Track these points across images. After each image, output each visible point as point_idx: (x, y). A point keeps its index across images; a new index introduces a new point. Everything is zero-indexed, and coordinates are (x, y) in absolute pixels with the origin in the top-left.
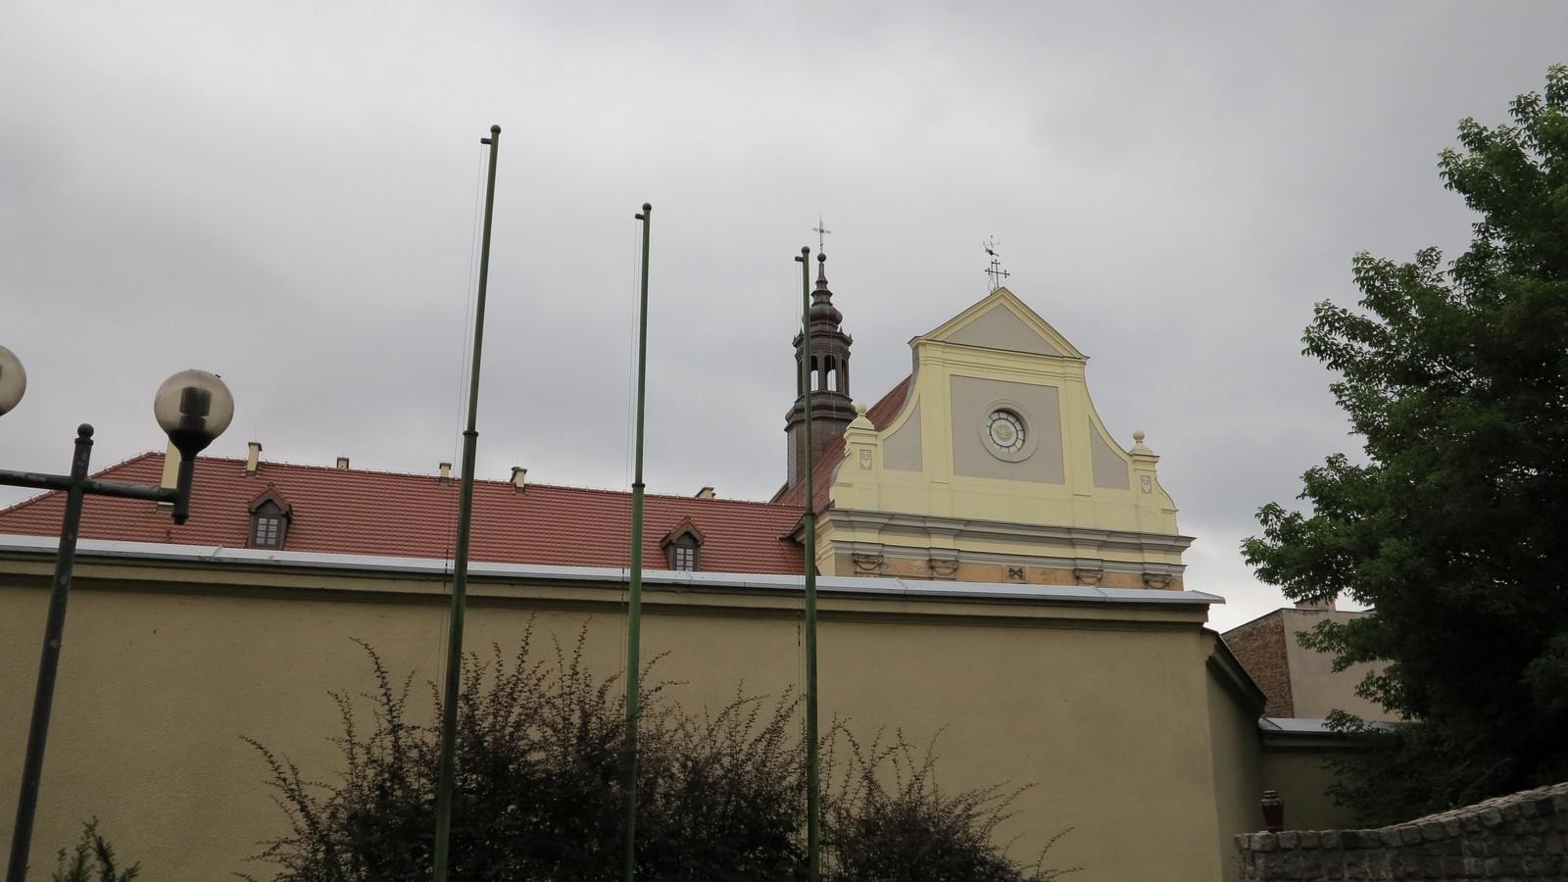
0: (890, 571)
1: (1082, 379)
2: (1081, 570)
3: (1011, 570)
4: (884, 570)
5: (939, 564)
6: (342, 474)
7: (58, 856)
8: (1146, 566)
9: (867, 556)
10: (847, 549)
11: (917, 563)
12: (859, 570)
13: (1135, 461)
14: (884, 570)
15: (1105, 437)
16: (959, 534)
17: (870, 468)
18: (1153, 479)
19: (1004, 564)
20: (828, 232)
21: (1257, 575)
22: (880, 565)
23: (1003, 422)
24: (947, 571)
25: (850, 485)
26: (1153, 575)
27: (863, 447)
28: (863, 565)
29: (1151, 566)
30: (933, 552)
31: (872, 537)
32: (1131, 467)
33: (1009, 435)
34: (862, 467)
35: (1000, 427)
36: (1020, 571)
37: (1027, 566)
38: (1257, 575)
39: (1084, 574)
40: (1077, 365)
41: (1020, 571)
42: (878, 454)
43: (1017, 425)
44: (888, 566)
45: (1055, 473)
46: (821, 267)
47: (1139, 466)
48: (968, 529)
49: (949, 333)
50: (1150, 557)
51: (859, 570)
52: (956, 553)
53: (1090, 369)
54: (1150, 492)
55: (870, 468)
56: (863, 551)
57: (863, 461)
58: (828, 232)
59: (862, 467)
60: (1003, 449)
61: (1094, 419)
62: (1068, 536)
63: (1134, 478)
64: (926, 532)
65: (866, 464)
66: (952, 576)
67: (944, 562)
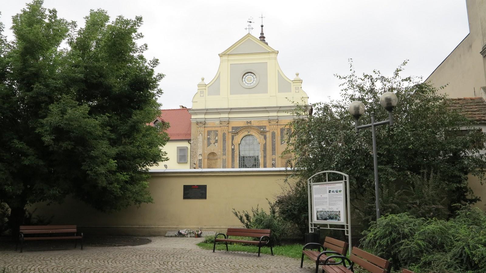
0: (208, 126)
1: (276, 59)
4: (206, 126)
8: (269, 117)
9: (201, 122)
11: (217, 123)
13: (293, 82)
16: (229, 113)
20: (262, 15)
25: (197, 102)
26: (272, 120)
27: (201, 90)
28: (199, 125)
30: (221, 119)
31: (202, 116)
33: (251, 80)
35: (248, 78)
36: (250, 122)
37: (253, 120)
39: (272, 121)
43: (252, 75)
44: (208, 124)
46: (262, 29)
47: (295, 84)
49: (231, 51)
50: (271, 114)
51: (198, 126)
52: (277, 117)
53: (279, 56)
55: (203, 96)
58: (262, 15)
59: (296, 92)
61: (279, 71)
63: (293, 88)
64: (219, 113)
65: (202, 95)
66: (227, 126)
67: (225, 121)
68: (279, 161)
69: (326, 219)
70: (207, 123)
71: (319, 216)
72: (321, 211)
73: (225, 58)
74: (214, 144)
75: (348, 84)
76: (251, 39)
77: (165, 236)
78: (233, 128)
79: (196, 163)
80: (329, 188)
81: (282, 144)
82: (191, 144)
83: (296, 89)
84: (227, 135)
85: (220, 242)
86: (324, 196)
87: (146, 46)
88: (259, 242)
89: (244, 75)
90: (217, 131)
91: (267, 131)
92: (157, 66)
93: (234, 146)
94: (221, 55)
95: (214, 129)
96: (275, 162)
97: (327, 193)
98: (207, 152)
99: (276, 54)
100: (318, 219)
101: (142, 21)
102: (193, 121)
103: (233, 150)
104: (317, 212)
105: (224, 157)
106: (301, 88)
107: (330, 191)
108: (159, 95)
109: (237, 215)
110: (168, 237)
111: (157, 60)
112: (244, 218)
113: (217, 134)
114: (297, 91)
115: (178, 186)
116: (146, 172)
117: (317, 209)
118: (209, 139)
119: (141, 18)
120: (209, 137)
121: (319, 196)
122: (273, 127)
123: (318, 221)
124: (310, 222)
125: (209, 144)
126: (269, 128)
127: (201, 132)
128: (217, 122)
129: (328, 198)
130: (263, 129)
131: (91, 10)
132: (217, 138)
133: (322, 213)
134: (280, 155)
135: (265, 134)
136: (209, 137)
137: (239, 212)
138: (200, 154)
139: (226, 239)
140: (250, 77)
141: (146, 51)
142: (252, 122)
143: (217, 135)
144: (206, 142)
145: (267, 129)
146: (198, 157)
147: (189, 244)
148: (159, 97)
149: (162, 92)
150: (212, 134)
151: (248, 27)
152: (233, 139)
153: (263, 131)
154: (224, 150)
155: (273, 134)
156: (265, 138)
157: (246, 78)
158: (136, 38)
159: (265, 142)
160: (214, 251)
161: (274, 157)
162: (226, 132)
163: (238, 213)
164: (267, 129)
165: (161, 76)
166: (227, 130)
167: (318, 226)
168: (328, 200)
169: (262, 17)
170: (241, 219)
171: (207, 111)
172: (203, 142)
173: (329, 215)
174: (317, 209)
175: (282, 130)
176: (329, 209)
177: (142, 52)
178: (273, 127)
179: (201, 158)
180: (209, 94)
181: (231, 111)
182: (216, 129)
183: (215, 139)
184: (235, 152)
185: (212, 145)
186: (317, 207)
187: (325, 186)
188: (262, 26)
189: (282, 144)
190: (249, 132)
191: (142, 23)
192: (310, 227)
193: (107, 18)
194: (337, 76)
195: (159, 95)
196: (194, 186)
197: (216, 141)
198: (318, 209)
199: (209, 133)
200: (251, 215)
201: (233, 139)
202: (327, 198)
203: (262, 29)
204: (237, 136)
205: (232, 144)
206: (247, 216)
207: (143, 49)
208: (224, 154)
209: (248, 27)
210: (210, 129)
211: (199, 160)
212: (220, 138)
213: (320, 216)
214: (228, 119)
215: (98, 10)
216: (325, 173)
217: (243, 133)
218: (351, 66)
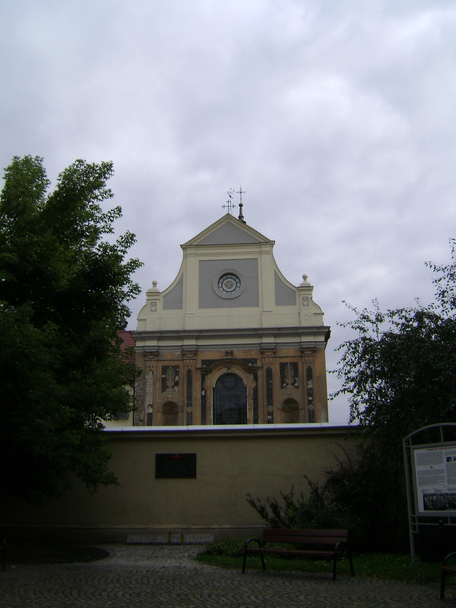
0: (163, 358)
2: (264, 349)
4: (160, 358)
5: (187, 353)
7: (304, 495)
8: (145, 348)
9: (151, 352)
10: (141, 350)
12: (147, 359)
14: (160, 358)
15: (283, 280)
17: (155, 310)
18: (309, 298)
19: (223, 350)
22: (157, 356)
24: (191, 356)
28: (149, 357)
29: (266, 345)
31: (154, 343)
32: (297, 294)
33: (232, 286)
35: (228, 282)
37: (235, 349)
40: (269, 246)
43: (234, 278)
44: (162, 356)
45: (254, 300)
46: (241, 209)
48: (201, 334)
51: (147, 359)
53: (276, 249)
54: (308, 305)
57: (304, 303)
62: (255, 333)
65: (154, 309)
66: (194, 358)
68: (277, 414)
69: (443, 508)
70: (162, 353)
71: (428, 503)
72: (432, 495)
73: (189, 251)
74: (173, 387)
75: (447, 279)
76: (232, 222)
77: (127, 544)
78: (204, 362)
79: (142, 418)
80: (446, 453)
81: (282, 387)
82: (134, 388)
83: (303, 300)
84: (194, 374)
85: (253, 553)
86: (436, 467)
87: (120, 211)
88: (333, 553)
89: (220, 280)
90: (178, 367)
91: (259, 368)
92: (132, 247)
93: (205, 392)
94: (184, 247)
95: (172, 363)
96: (273, 418)
97: (443, 462)
98: (160, 401)
99: (272, 246)
100: (426, 508)
101: (112, 171)
102: (137, 351)
103: (204, 398)
104: (425, 496)
105: (189, 409)
106: (312, 298)
107: (448, 459)
108: (134, 295)
109: (253, 504)
110: (132, 544)
111: (133, 235)
112: (269, 510)
113: (178, 372)
114: (305, 303)
115: (147, 456)
116: (99, 432)
117: (423, 491)
118: (164, 380)
119: (111, 165)
120: (164, 376)
121: (427, 468)
122: (269, 360)
123: (428, 511)
124: (410, 515)
125: (164, 388)
126: (262, 362)
127: (151, 368)
128: (178, 353)
129: (445, 471)
130: (253, 364)
131: (15, 158)
132: (177, 377)
133: (435, 497)
134: (280, 406)
135: (256, 372)
136: (164, 376)
137: (259, 500)
138: (150, 405)
139: (262, 549)
140: (231, 282)
141: (118, 219)
142: (235, 353)
143: (177, 373)
144: (159, 385)
145: (259, 364)
146: (146, 409)
147: (181, 561)
148: (134, 298)
149: (140, 289)
150: (170, 371)
151: (226, 204)
152: (203, 380)
153: (251, 367)
154: (190, 397)
155: (269, 372)
156: (256, 378)
157: (224, 282)
158: (100, 197)
159: (254, 385)
160: (244, 572)
161: (270, 408)
162: (193, 369)
163: (256, 501)
164: (259, 364)
165: (135, 264)
166: (193, 365)
167: (441, 521)
168: (445, 474)
169: (241, 192)
170: (262, 511)
171: (161, 335)
172: (154, 384)
173: (449, 501)
174: (423, 491)
175: (283, 366)
176: (449, 490)
177: (112, 221)
178: (269, 360)
179: (151, 410)
180: (166, 307)
181: (200, 334)
182: (176, 363)
183: (174, 379)
184: (208, 401)
185: (170, 389)
186: (425, 487)
187: (438, 450)
188: (241, 205)
189: (282, 387)
190: (229, 369)
191: (113, 173)
192: (410, 523)
193: (38, 173)
194: (431, 266)
195: (134, 295)
196: (174, 455)
197: (177, 384)
198: (426, 490)
199: (165, 369)
200: (282, 504)
201: (203, 380)
202: (443, 470)
203: (241, 209)
204: (210, 376)
205: (203, 389)
206: (275, 508)
207: (113, 215)
208: (190, 404)
209: (226, 204)
210: (166, 363)
211: (148, 414)
212: (182, 377)
213: (431, 503)
214: (196, 347)
215: (26, 158)
216: (439, 427)
217: (219, 370)
218: (453, 251)
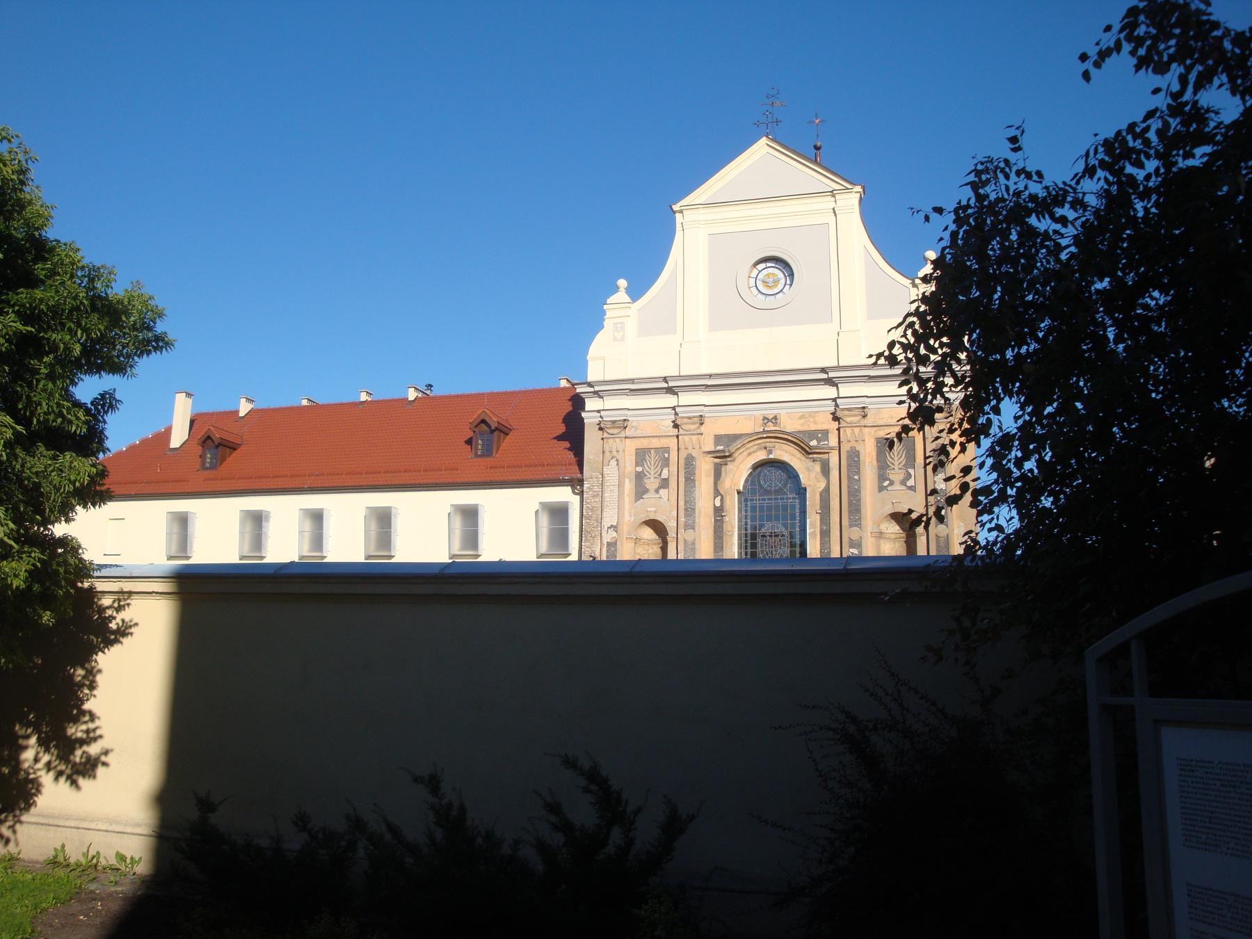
3: (765, 418)
4: (628, 432)
5: (846, 412)
6: (315, 408)
9: (614, 422)
21: (583, 813)
23: (771, 270)
33: (776, 282)
34: (615, 339)
35: (768, 275)
36: (775, 418)
37: (783, 412)
38: (583, 813)
41: (775, 418)
42: (631, 325)
56: (608, 417)
60: (760, 296)
67: (689, 418)
